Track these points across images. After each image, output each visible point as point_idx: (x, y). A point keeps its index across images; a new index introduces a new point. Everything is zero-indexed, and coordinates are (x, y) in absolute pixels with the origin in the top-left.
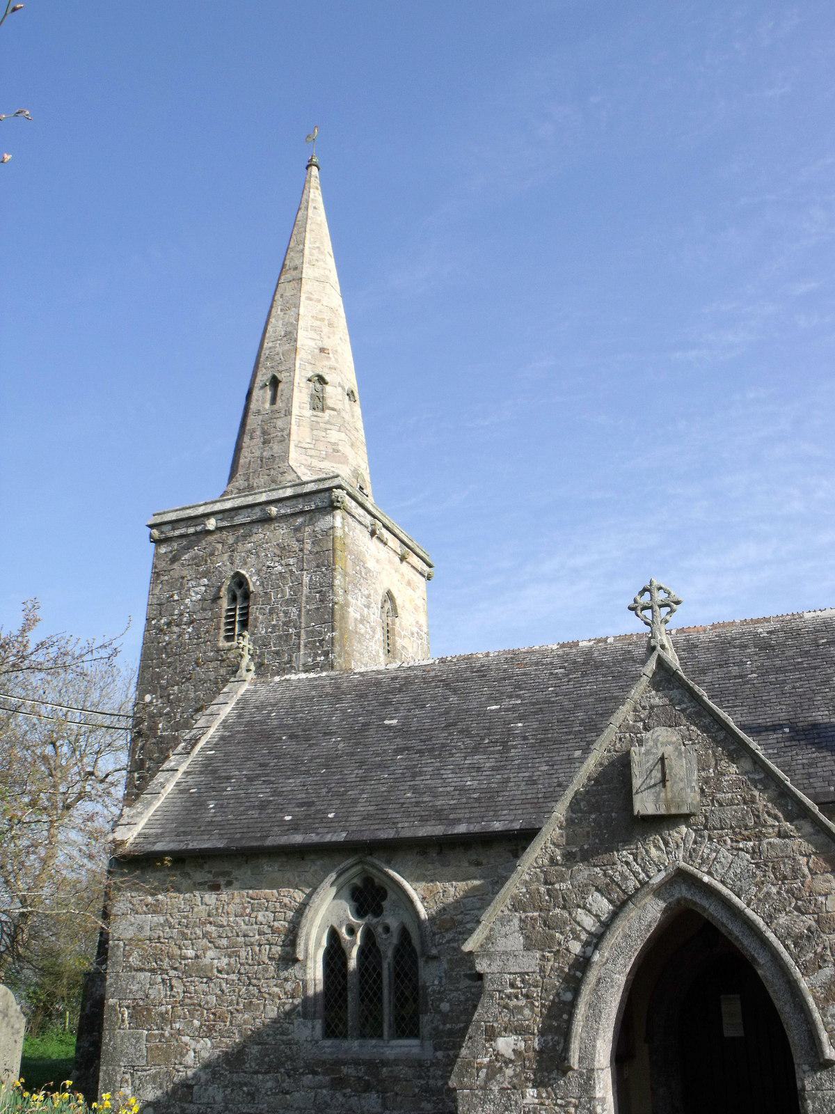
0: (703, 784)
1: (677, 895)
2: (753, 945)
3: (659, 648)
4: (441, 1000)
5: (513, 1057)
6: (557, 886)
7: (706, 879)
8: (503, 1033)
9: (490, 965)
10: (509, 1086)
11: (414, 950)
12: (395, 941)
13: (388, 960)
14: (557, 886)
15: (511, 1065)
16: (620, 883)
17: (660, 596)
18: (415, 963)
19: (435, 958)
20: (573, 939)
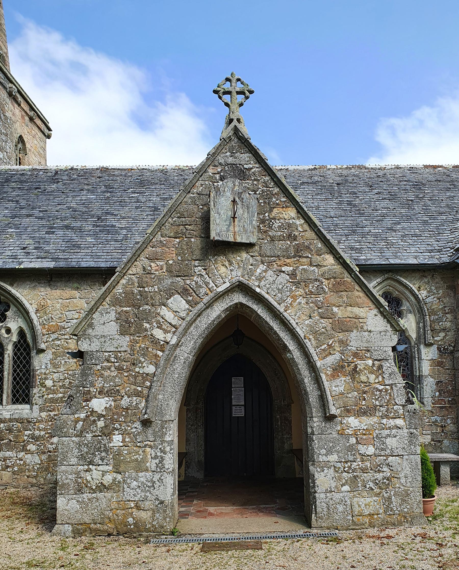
0: (260, 224)
1: (236, 301)
2: (286, 337)
3: (235, 120)
4: (46, 379)
5: (104, 413)
6: (146, 289)
7: (258, 290)
8: (98, 395)
9: (90, 345)
10: (100, 434)
11: (28, 345)
12: (15, 338)
13: (8, 352)
14: (146, 289)
15: (102, 419)
16: (195, 289)
17: (239, 87)
18: (29, 354)
19: (43, 351)
20: (158, 327)
